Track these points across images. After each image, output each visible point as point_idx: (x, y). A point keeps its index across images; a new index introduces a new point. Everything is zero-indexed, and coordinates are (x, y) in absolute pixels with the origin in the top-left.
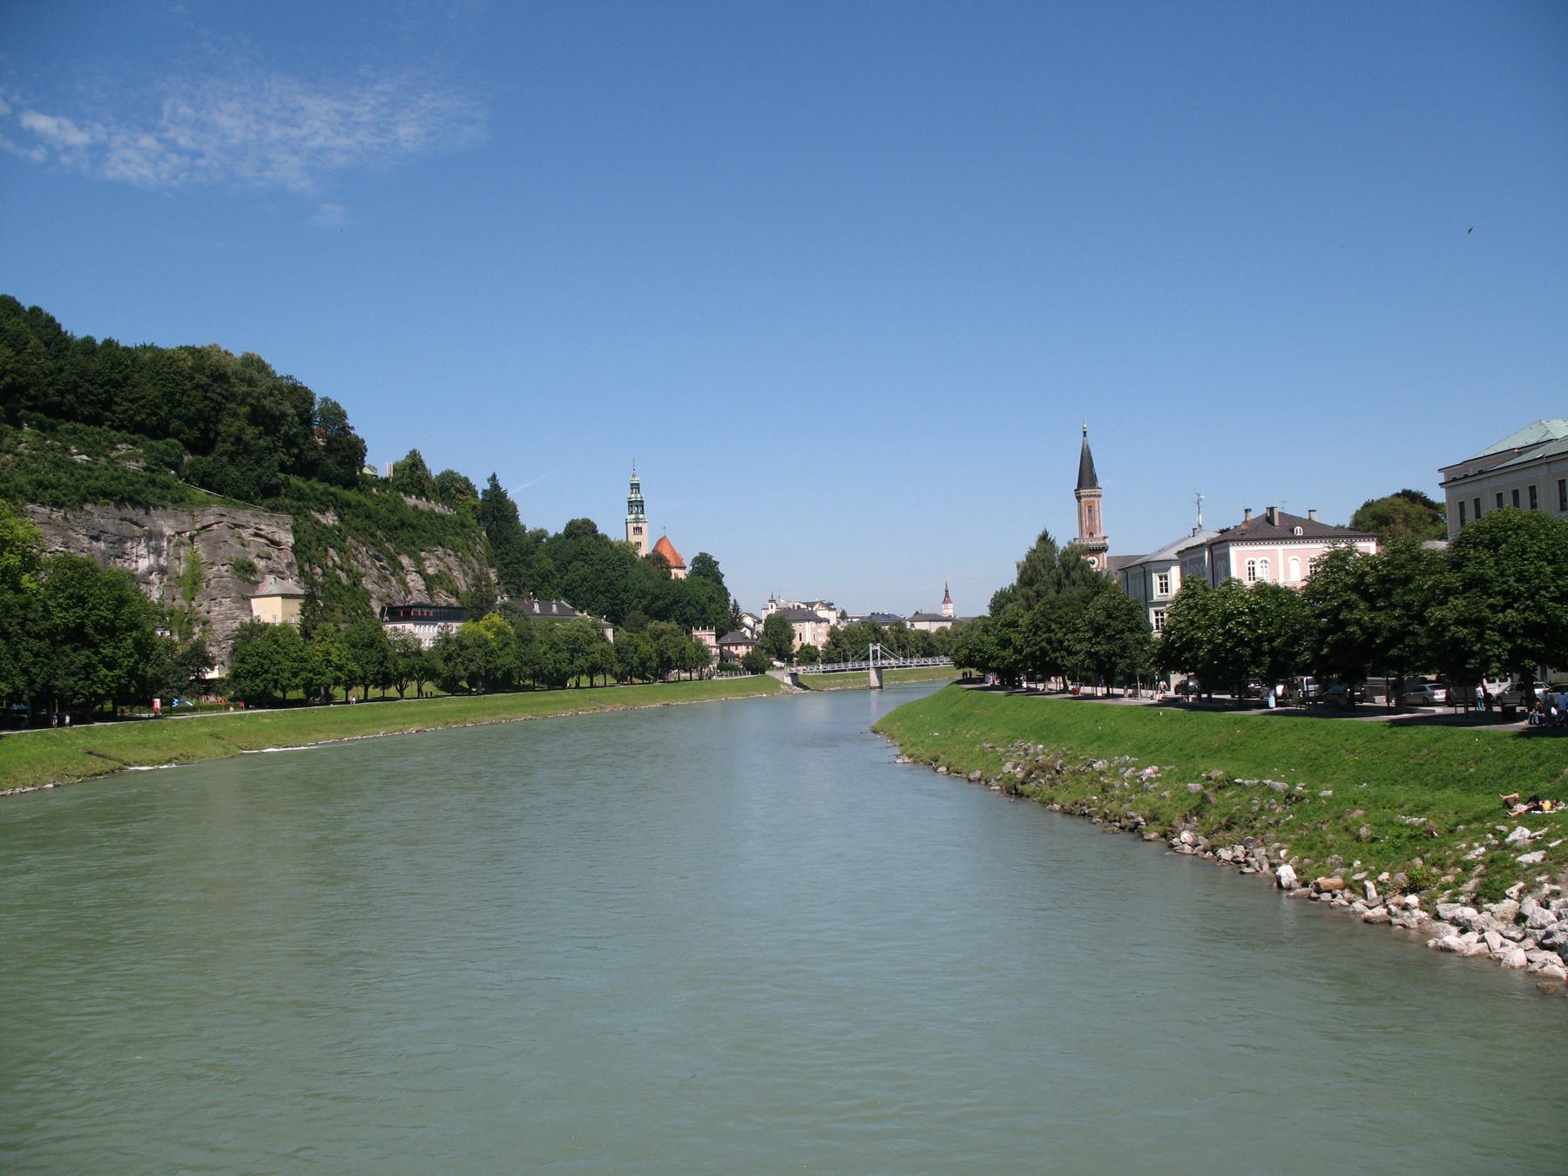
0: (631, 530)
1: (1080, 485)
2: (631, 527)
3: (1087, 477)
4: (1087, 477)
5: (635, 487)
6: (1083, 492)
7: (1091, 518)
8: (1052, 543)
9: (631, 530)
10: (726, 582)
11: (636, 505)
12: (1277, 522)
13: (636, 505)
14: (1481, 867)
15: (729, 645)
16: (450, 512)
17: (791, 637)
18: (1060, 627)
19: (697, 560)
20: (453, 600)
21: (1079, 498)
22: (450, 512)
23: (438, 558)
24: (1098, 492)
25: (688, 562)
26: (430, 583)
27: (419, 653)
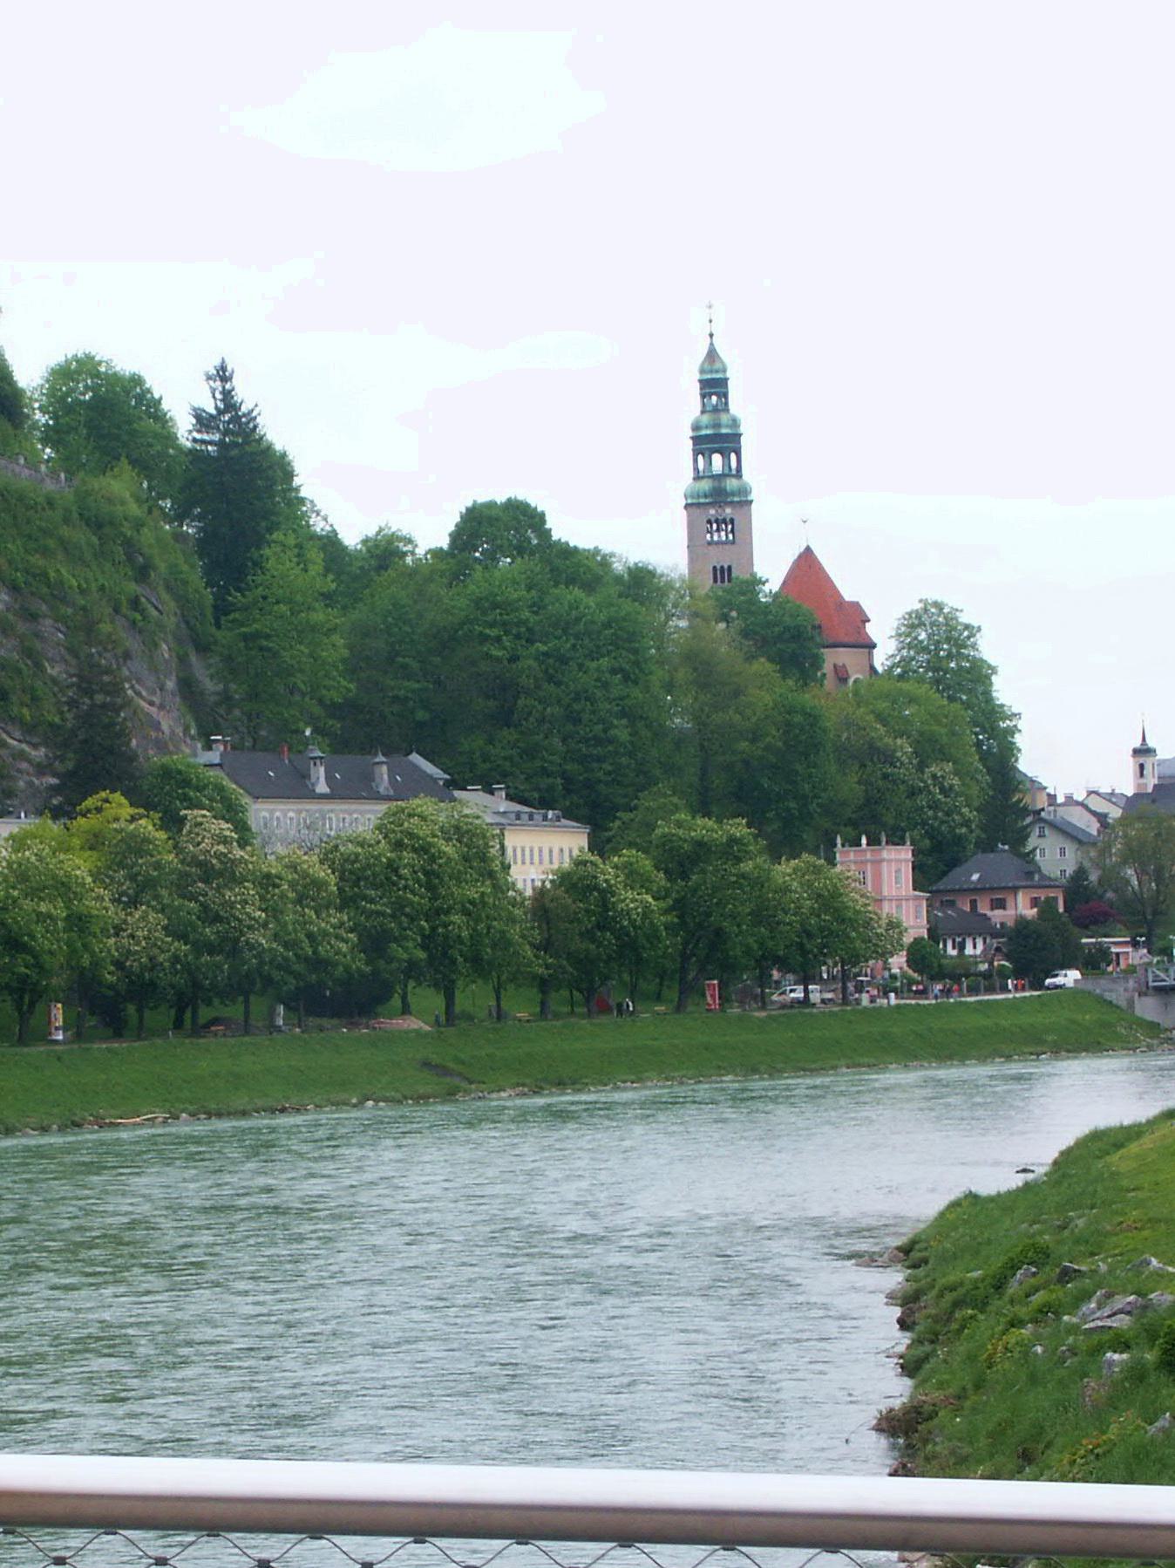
19: (914, 621)
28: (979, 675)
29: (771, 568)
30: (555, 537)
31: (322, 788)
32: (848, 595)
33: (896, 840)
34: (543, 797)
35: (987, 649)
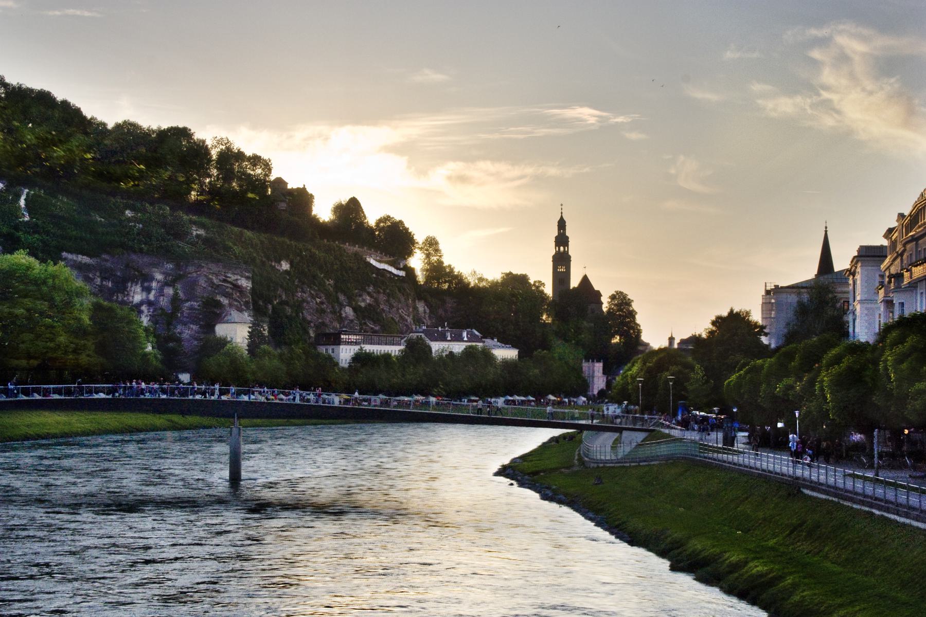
19: (613, 297)
28: (632, 314)
29: (575, 282)
30: (110, 126)
31: (449, 338)
32: (596, 288)
33: (598, 361)
34: (506, 341)
35: (635, 306)
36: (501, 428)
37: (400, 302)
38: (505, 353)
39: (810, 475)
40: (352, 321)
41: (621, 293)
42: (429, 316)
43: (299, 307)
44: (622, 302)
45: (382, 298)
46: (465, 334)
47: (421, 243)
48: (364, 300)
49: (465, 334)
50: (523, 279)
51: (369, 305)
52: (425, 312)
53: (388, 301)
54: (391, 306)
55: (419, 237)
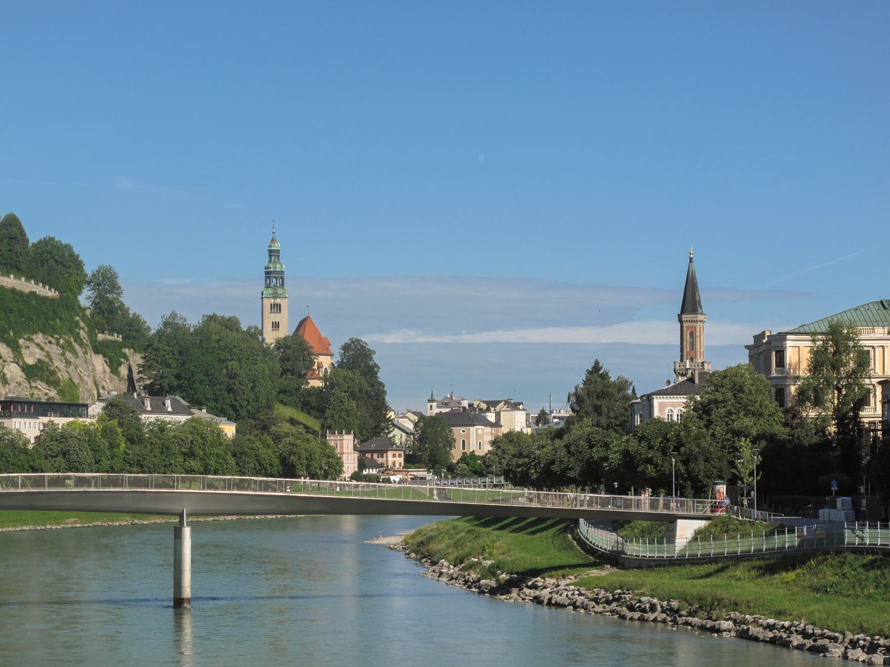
0: (267, 308)
1: (683, 311)
2: (268, 303)
3: (690, 303)
4: (690, 303)
5: (273, 254)
6: (685, 317)
7: (693, 344)
8: (604, 376)
9: (267, 308)
10: (382, 376)
11: (273, 278)
12: (697, 381)
13: (273, 278)
14: (463, 534)
15: (372, 452)
16: (51, 293)
17: (450, 443)
18: (604, 451)
19: (346, 348)
20: (53, 393)
21: (681, 322)
22: (51, 293)
23: (38, 345)
24: (700, 317)
25: (336, 349)
26: (31, 372)
27: (25, 451)
36: (18, 512)
37: (77, 356)
38: (229, 430)
39: (396, 575)
40: (20, 384)
41: (357, 340)
42: (110, 378)
43: (834, 506)
44: (128, 308)
45: (55, 350)
46: (168, 403)
47: (90, 275)
48: (31, 354)
49: (168, 403)
50: (231, 324)
51: (40, 361)
52: (105, 372)
53: (63, 355)
54: (68, 363)
55: (89, 269)
